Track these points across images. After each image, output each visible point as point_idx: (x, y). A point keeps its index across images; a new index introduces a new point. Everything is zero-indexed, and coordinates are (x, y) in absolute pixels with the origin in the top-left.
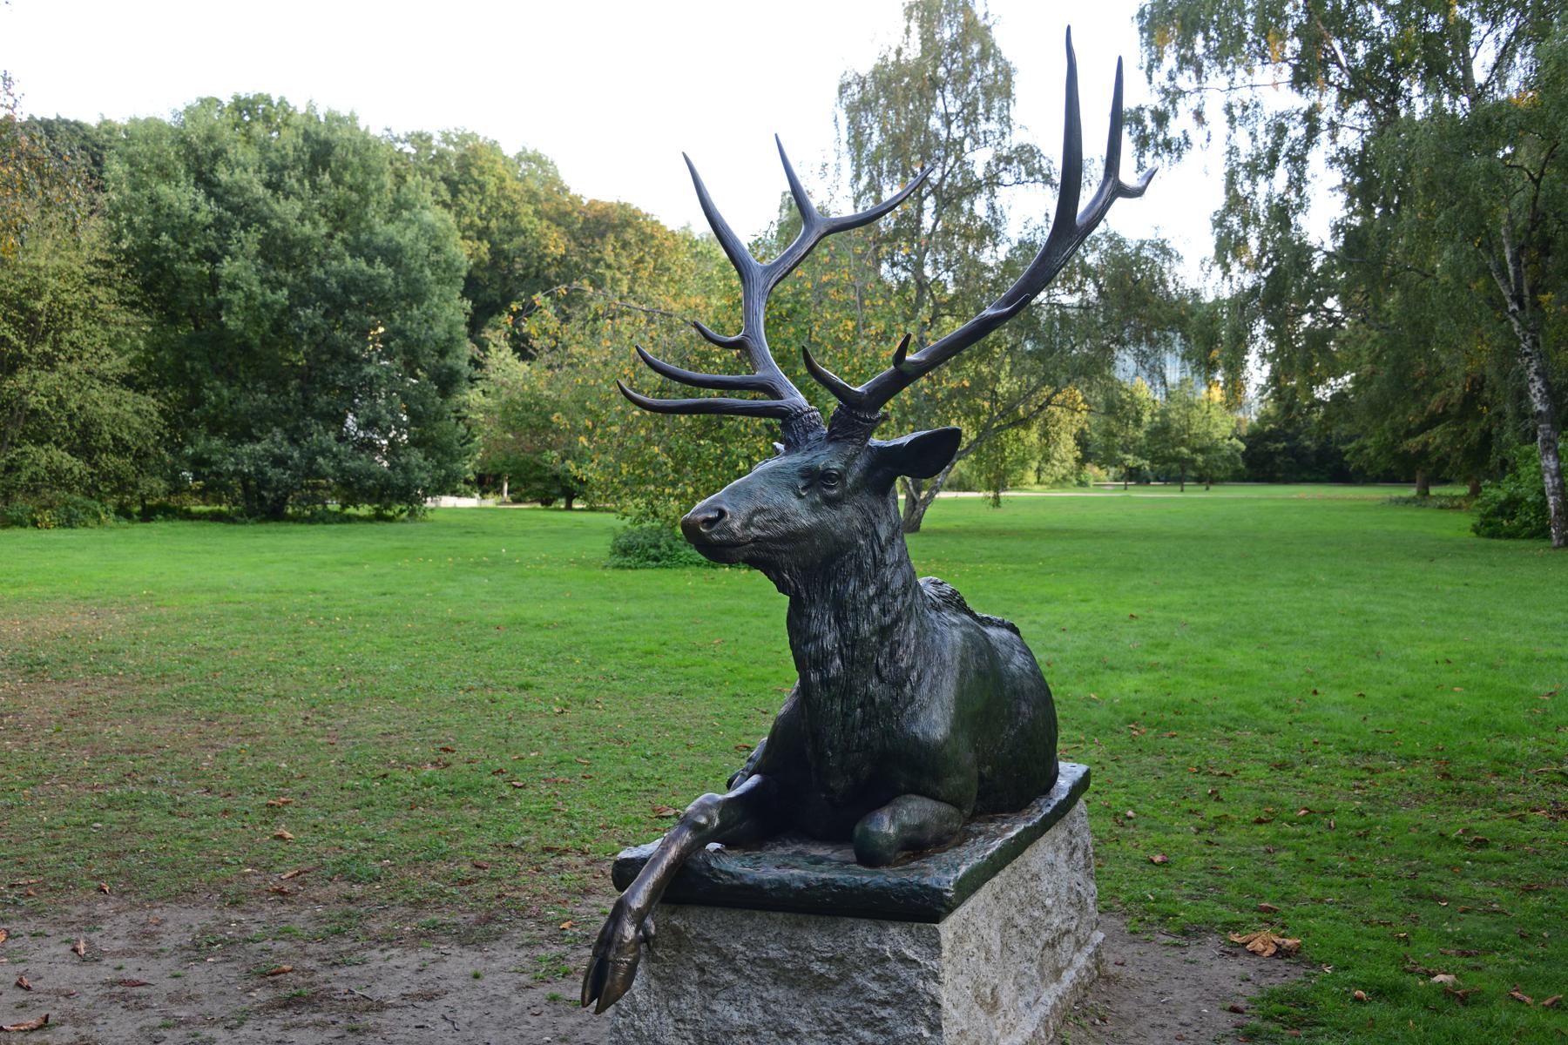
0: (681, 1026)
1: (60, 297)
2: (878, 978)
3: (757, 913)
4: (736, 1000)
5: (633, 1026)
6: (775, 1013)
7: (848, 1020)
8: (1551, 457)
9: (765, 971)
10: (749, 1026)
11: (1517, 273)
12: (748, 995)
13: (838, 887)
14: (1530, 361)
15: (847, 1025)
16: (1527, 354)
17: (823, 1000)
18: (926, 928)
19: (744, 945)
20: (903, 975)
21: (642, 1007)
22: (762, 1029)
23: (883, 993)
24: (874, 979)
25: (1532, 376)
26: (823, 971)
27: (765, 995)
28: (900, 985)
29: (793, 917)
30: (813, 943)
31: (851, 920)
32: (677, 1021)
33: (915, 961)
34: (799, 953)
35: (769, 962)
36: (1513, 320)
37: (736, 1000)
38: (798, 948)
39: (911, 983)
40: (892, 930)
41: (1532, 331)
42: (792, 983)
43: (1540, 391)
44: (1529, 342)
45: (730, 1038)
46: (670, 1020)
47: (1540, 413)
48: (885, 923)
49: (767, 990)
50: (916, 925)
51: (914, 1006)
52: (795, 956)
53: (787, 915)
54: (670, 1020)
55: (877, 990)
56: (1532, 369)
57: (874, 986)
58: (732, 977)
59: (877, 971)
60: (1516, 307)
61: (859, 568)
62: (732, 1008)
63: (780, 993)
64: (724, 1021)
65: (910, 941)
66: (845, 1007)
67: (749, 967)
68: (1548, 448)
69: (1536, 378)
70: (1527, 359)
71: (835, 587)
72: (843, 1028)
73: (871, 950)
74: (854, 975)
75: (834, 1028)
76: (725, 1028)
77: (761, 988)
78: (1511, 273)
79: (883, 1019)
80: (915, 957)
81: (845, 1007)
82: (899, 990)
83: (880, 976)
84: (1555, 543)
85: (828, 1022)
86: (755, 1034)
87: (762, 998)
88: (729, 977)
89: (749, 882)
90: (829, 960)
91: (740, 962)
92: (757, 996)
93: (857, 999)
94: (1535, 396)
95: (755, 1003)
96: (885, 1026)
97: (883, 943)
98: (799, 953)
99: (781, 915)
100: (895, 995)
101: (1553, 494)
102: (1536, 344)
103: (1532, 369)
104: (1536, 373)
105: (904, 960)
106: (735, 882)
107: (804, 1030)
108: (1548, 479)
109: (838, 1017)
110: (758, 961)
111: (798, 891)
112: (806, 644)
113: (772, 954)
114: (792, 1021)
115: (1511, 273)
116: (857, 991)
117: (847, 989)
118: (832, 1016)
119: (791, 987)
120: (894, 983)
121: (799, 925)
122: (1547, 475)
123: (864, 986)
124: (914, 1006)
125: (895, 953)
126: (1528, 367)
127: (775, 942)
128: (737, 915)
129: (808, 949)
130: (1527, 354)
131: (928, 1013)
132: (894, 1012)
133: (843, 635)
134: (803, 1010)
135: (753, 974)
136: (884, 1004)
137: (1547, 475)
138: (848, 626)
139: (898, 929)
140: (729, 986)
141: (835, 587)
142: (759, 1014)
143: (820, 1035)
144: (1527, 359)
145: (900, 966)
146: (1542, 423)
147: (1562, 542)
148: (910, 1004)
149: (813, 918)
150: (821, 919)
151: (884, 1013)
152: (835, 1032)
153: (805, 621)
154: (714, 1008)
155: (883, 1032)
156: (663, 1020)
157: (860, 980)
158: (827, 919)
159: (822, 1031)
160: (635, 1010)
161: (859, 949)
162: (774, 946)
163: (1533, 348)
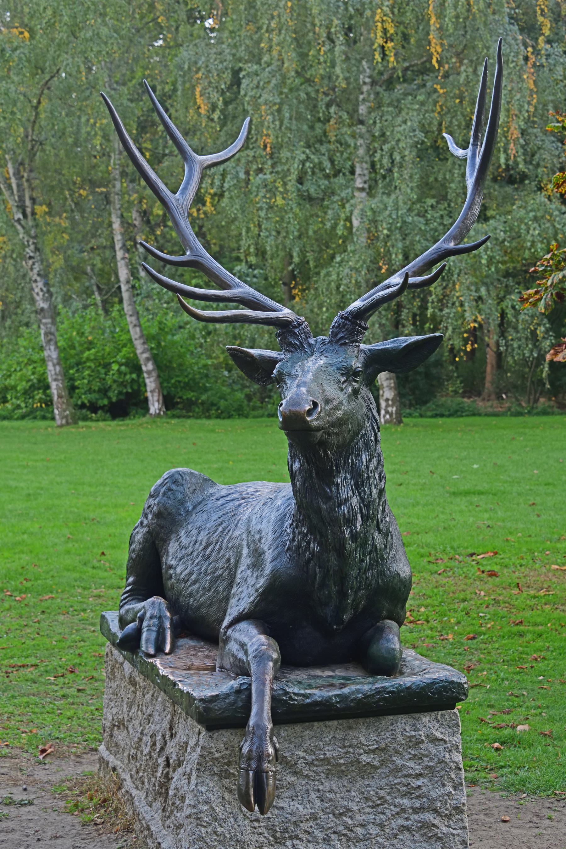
0: (256, 824)
1: (318, 249)
2: (414, 757)
3: (316, 724)
4: (297, 796)
5: (215, 832)
6: (331, 800)
7: (389, 794)
8: (52, 348)
9: (320, 769)
10: (312, 814)
11: (19, 186)
12: (307, 790)
13: (388, 693)
14: (34, 264)
15: (388, 798)
16: (31, 258)
17: (366, 783)
18: (447, 713)
19: (305, 751)
20: (434, 751)
21: (220, 816)
22: (321, 814)
23: (418, 769)
24: (410, 759)
25: (35, 277)
26: (369, 760)
27: (321, 787)
28: (432, 759)
29: (345, 723)
30: (363, 739)
31: (391, 717)
32: (252, 821)
33: (442, 740)
34: (351, 750)
35: (326, 761)
36: (19, 227)
37: (297, 796)
38: (350, 746)
39: (441, 756)
40: (424, 720)
41: (35, 237)
42: (341, 775)
43: (42, 290)
44: (32, 247)
45: (299, 826)
46: (247, 822)
47: (42, 309)
48: (417, 715)
49: (322, 784)
50: (440, 713)
51: (443, 773)
52: (348, 752)
53: (341, 721)
54: (247, 822)
55: (415, 767)
56: (35, 271)
57: (411, 764)
58: (293, 779)
59: (413, 753)
60: (20, 216)
61: (367, 445)
62: (296, 803)
63: (334, 784)
64: (292, 814)
65: (437, 726)
66: (387, 785)
67: (307, 768)
68: (50, 340)
69: (38, 279)
70: (30, 262)
71: (352, 460)
72: (386, 801)
73: (409, 737)
74: (394, 758)
75: (379, 802)
76: (294, 819)
77: (316, 783)
78: (14, 186)
79: (419, 787)
80: (441, 736)
81: (387, 785)
82: (431, 764)
83: (415, 755)
84: (59, 422)
85: (374, 798)
86: (316, 819)
87: (319, 791)
88: (291, 779)
89: (319, 699)
90: (373, 751)
91: (301, 765)
92: (313, 790)
93: (396, 777)
94: (38, 294)
95: (313, 795)
96: (420, 792)
97: (419, 730)
98: (351, 750)
99: (335, 722)
100: (427, 767)
101: (56, 380)
102: (37, 249)
103: (35, 271)
104: (39, 275)
105: (434, 740)
106: (308, 701)
107: (355, 808)
108: (50, 367)
109: (382, 793)
110: (315, 762)
111: (359, 701)
112: (339, 506)
113: (328, 754)
114: (346, 803)
115: (14, 186)
116: (397, 770)
117: (387, 770)
118: (377, 793)
119: (340, 778)
120: (425, 759)
121: (350, 728)
122: (50, 364)
123: (404, 765)
124: (443, 773)
125: (427, 736)
126: (32, 269)
127: (330, 744)
128: (298, 728)
129: (360, 745)
130: (31, 258)
131: (453, 776)
132: (425, 781)
133: (361, 498)
134: (353, 794)
135: (311, 773)
136: (418, 776)
137: (50, 364)
138: (364, 491)
139: (428, 718)
140: (292, 785)
141: (352, 460)
142: (318, 803)
143: (367, 810)
144: (30, 262)
145: (430, 745)
146: (44, 317)
147: (64, 421)
148: (439, 772)
149: (361, 720)
150: (368, 720)
151: (419, 783)
152: (378, 805)
153: (334, 489)
154: (282, 805)
155: (418, 797)
156: (240, 823)
157: (399, 762)
158: (372, 719)
159: (369, 807)
160: (216, 820)
161: (400, 738)
162: (330, 748)
163: (35, 252)
